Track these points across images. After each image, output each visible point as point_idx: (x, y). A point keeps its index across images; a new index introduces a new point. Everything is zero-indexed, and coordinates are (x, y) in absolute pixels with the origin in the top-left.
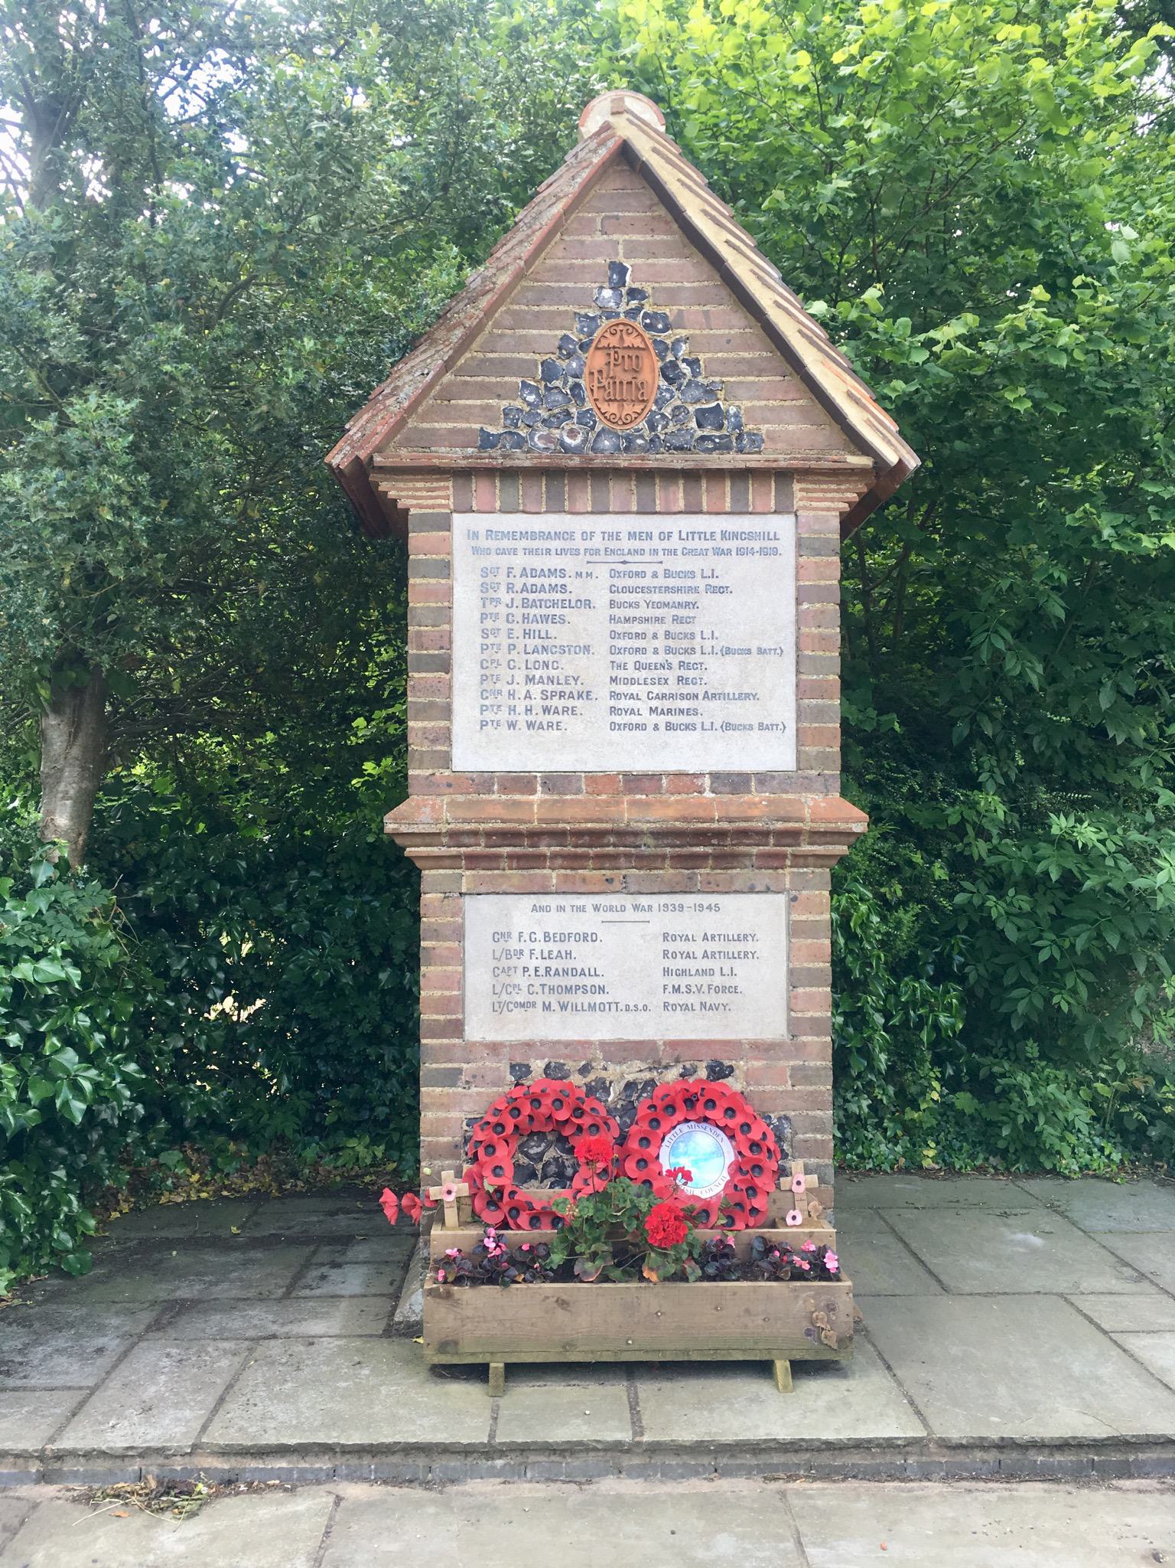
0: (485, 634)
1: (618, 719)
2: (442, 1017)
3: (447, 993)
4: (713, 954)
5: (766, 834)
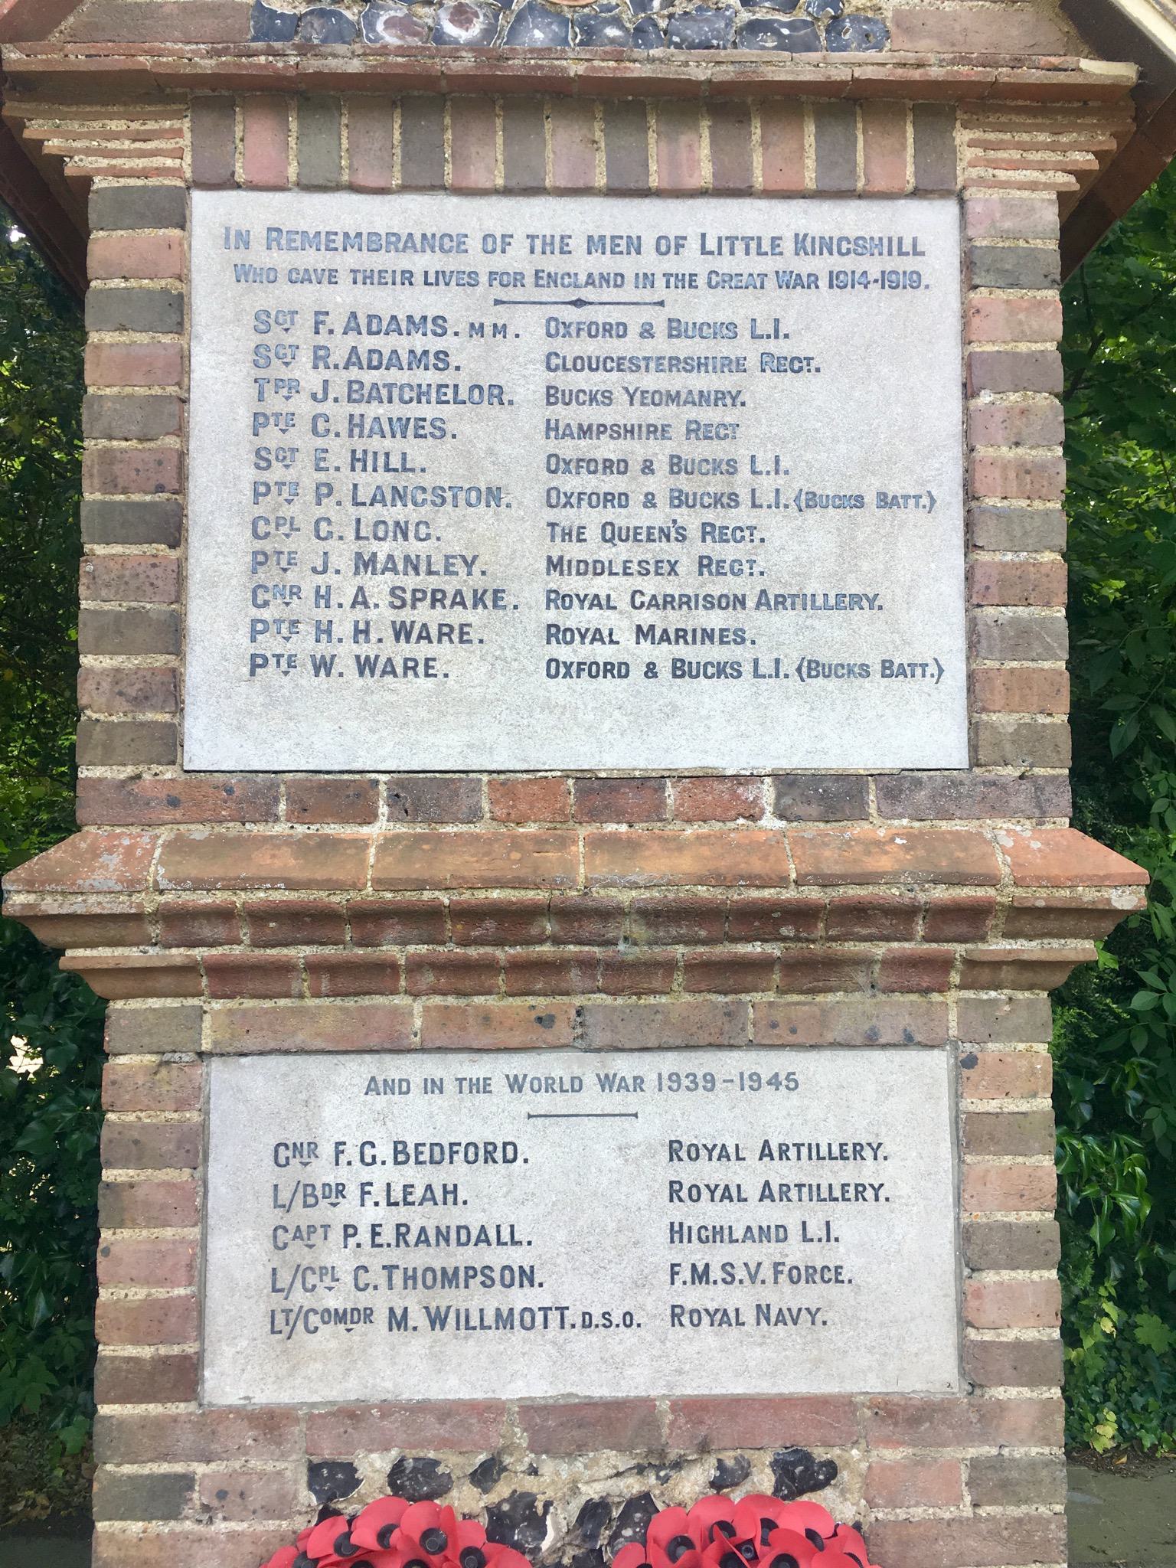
0: (262, 459)
1: (564, 653)
2: (146, 1352)
3: (160, 1293)
4: (785, 1189)
5: (905, 914)
